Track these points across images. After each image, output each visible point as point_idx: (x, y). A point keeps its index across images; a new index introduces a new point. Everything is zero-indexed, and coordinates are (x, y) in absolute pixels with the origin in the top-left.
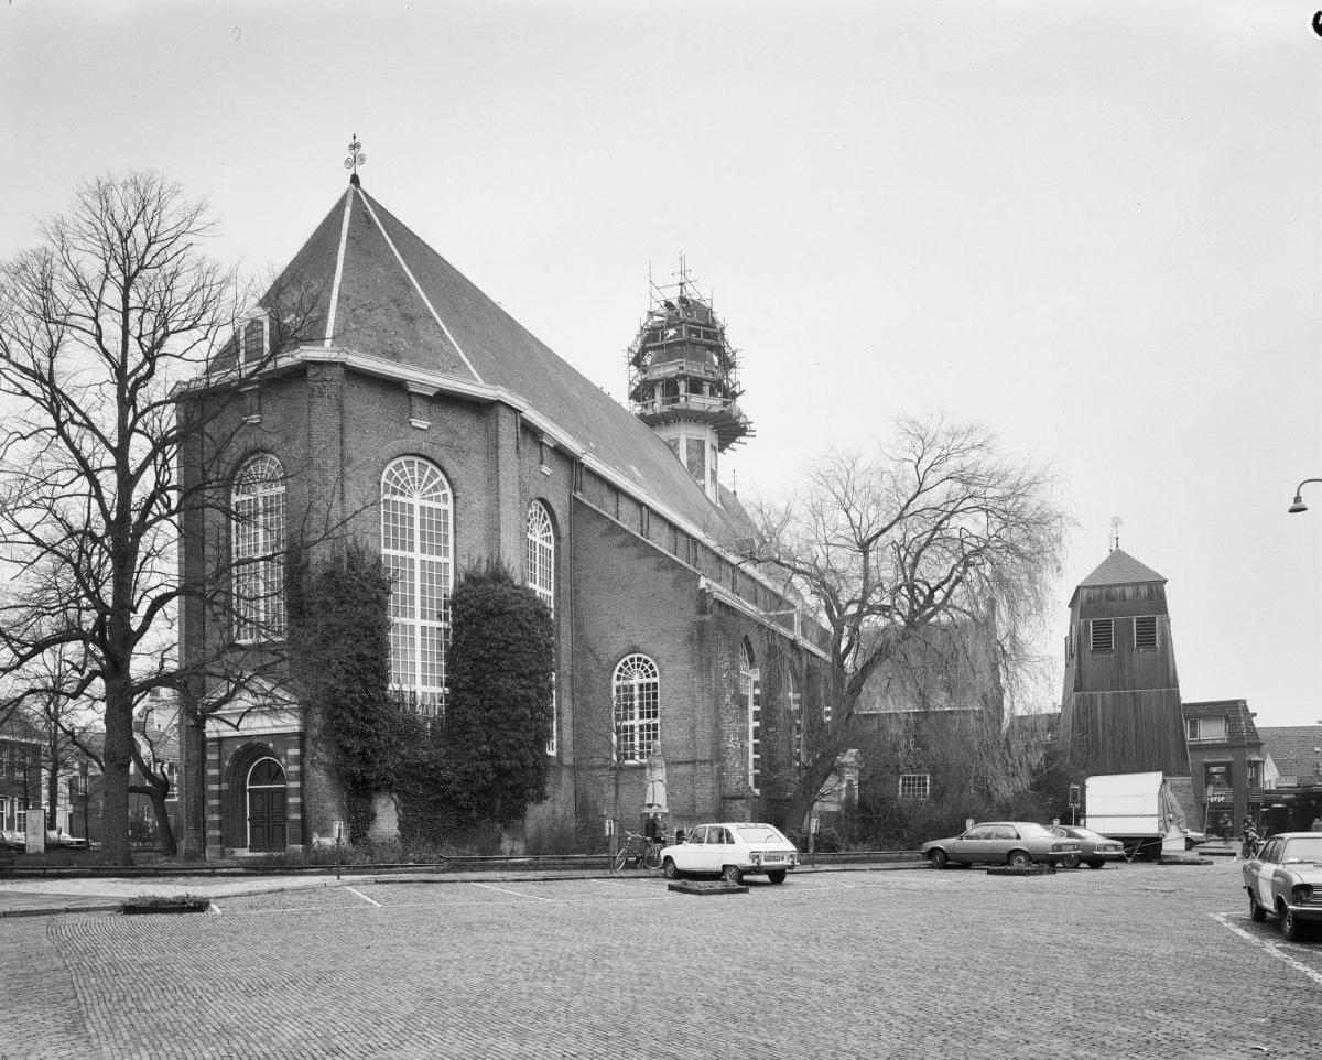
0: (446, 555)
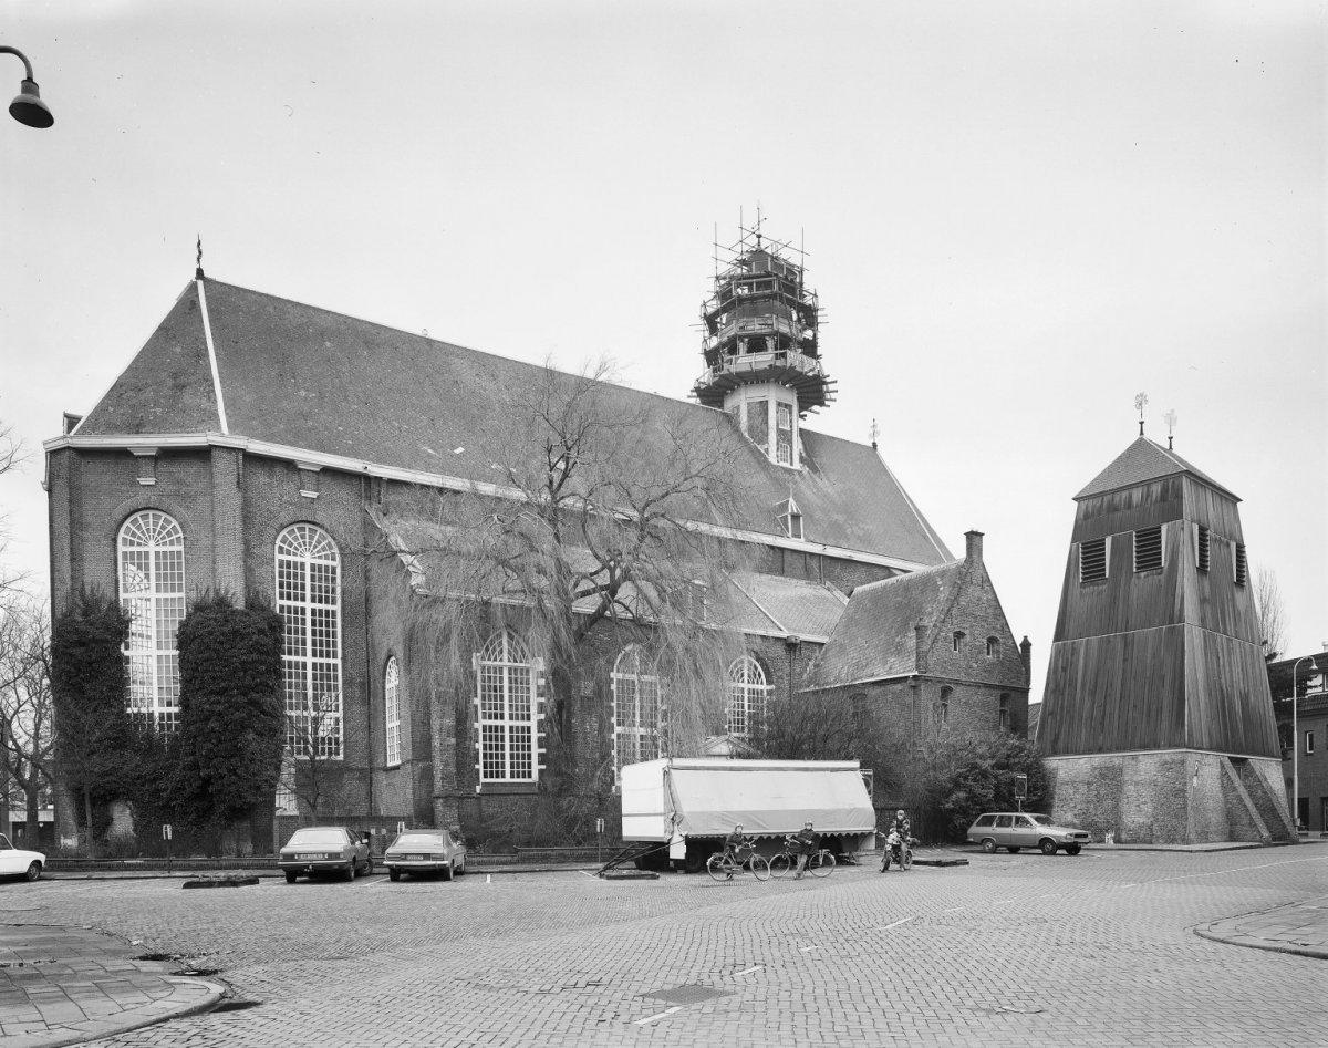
0: (334, 603)
